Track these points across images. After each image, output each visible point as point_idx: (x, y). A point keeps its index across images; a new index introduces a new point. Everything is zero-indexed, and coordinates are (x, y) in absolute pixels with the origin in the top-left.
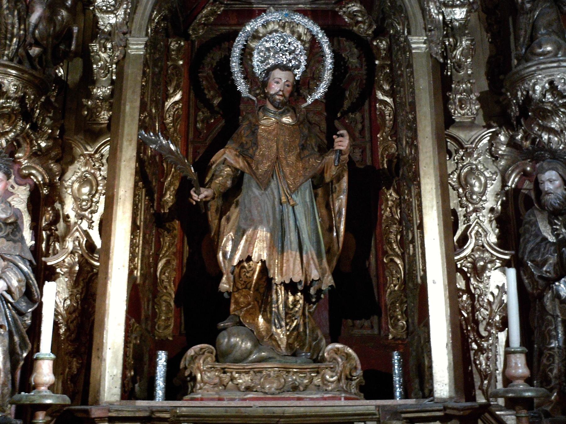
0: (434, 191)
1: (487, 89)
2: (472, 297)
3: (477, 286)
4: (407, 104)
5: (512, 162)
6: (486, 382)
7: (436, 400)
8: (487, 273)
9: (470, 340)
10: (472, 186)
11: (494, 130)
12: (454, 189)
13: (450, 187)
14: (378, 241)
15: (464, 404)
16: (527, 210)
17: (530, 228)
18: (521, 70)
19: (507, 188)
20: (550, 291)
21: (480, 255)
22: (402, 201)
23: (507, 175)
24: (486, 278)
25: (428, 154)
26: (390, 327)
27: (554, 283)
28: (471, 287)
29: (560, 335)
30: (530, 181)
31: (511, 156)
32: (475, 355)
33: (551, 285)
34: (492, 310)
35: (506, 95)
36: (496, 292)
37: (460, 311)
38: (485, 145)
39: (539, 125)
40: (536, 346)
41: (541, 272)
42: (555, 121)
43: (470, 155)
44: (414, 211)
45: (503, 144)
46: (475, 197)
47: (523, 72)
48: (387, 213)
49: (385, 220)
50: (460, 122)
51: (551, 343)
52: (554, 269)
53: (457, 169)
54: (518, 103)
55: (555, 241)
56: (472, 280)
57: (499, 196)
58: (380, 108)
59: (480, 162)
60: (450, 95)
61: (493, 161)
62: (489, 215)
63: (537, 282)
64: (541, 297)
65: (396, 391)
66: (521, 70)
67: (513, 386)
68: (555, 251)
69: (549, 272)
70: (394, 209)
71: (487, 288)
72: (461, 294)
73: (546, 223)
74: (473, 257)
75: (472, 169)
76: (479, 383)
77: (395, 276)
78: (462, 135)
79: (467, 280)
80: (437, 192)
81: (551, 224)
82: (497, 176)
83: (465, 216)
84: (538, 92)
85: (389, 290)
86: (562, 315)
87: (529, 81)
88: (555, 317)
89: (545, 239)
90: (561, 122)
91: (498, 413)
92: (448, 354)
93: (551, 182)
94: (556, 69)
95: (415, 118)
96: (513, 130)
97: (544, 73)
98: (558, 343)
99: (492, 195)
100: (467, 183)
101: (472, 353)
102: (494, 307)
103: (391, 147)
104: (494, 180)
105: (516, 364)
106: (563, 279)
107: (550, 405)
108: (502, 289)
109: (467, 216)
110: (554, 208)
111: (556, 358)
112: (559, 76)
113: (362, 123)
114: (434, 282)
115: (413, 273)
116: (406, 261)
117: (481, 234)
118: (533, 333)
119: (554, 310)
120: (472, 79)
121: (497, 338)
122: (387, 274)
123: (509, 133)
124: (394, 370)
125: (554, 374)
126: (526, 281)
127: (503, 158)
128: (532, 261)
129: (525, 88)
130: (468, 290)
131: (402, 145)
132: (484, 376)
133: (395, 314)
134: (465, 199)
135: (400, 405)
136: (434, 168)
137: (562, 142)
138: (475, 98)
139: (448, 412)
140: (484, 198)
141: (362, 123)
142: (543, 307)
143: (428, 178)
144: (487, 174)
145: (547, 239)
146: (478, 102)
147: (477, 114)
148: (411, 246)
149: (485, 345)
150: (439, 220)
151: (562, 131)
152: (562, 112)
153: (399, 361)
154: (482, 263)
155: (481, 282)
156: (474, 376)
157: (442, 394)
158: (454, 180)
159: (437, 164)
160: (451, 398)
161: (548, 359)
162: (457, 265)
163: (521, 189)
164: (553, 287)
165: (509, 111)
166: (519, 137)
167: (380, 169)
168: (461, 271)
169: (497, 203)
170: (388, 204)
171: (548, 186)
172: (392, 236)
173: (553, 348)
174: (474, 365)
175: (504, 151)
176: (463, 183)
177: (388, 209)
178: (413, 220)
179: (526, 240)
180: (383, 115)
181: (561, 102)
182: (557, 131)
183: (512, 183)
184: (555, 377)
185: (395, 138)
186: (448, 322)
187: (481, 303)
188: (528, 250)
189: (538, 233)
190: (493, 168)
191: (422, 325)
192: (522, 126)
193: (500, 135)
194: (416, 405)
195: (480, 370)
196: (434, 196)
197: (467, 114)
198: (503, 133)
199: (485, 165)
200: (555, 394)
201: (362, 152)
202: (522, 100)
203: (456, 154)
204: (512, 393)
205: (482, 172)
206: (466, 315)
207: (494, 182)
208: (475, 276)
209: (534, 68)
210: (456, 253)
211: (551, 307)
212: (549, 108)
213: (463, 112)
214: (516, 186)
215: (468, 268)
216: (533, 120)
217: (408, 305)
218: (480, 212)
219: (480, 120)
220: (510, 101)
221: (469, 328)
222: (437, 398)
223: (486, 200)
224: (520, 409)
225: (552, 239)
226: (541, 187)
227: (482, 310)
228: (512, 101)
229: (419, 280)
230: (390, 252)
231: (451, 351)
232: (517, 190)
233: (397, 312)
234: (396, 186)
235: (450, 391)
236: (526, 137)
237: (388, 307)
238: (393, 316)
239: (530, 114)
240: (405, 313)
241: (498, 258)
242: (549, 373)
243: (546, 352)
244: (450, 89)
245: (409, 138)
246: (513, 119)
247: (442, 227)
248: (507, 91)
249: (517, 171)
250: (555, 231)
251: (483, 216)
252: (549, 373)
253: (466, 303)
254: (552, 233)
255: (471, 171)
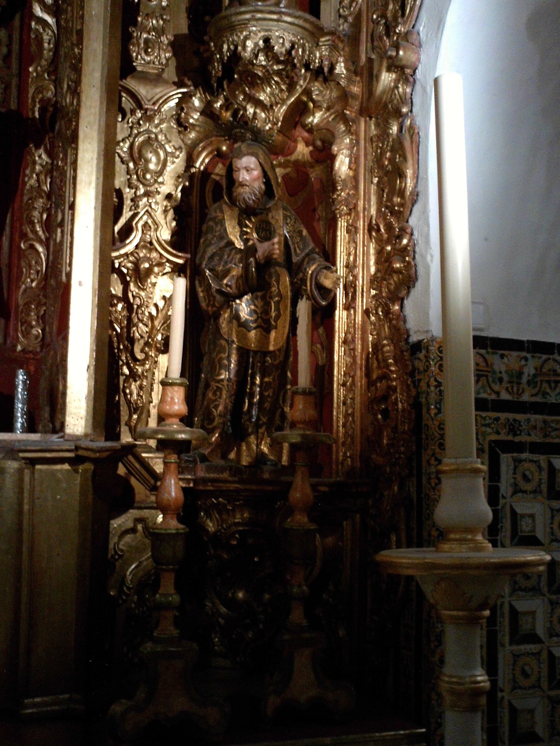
0: (95, 162)
1: (185, 31)
2: (129, 307)
3: (136, 293)
4: (74, 32)
5: (204, 137)
6: (135, 417)
7: (66, 437)
8: (153, 279)
9: (121, 363)
10: (147, 161)
11: (185, 90)
12: (123, 162)
13: (117, 158)
14: (15, 218)
15: (102, 444)
16: (215, 201)
17: (214, 226)
18: (231, 15)
19: (193, 170)
20: (229, 311)
21: (145, 255)
22: (55, 167)
23: (195, 153)
24: (150, 285)
25: (93, 110)
26: (20, 335)
27: (234, 301)
28: (130, 295)
29: (232, 365)
30: (224, 164)
31: (205, 130)
32: (125, 381)
33: (231, 303)
34: (153, 326)
35: (209, 45)
36: (161, 304)
37: (111, 323)
38: (171, 109)
39: (245, 93)
40: (203, 376)
41: (221, 285)
42: (264, 92)
43: (149, 118)
44: (68, 185)
45: (195, 110)
46: (148, 176)
47: (234, 19)
48: (33, 182)
49: (28, 190)
50: (142, 72)
51: (221, 374)
52: (236, 283)
53: (130, 136)
54: (222, 58)
55: (242, 248)
56: (132, 286)
57: (180, 180)
58: (37, 30)
59: (161, 130)
60: (134, 31)
61: (180, 132)
62: (165, 203)
63: (214, 297)
64: (217, 316)
65: (17, 421)
66: (231, 15)
67: (165, 425)
68: (241, 261)
69: (230, 287)
70: (42, 177)
71: (150, 298)
72: (115, 302)
73: (235, 222)
74: (136, 255)
75: (149, 138)
76: (126, 418)
77: (34, 268)
78: (142, 91)
79: (126, 285)
80: (98, 164)
81: (241, 225)
82: (181, 152)
83: (132, 200)
84: (249, 49)
85: (23, 286)
86: (239, 341)
87: (240, 32)
88: (230, 343)
89: (231, 244)
90: (272, 94)
91: (144, 455)
92: (89, 379)
93: (248, 170)
94: (275, 23)
95: (81, 55)
96: (212, 94)
97: (260, 25)
98: (229, 375)
99: (171, 177)
100: (141, 155)
101: (122, 378)
102: (156, 323)
103: (48, 90)
104: (177, 158)
105: (172, 398)
106: (246, 297)
107: (208, 448)
108: (168, 301)
109: (135, 200)
110: (247, 206)
111: (224, 392)
112: (277, 34)
113: (9, 46)
114: (80, 284)
115: (57, 267)
116: (51, 249)
117: (150, 227)
118: (202, 360)
119: (230, 335)
120: (167, 15)
121: (156, 362)
122: (23, 264)
123: (206, 97)
124: (17, 393)
125: (218, 412)
126: (201, 294)
127: (194, 130)
128: (210, 270)
129: (233, 40)
130: (125, 298)
131: (62, 89)
132: (134, 408)
133: (29, 319)
134: (135, 177)
135: (19, 441)
136: (99, 130)
137: (269, 120)
138: (166, 42)
139: (80, 452)
140: (161, 179)
141: (9, 46)
142: (218, 329)
143: (90, 143)
144: (169, 150)
145: (233, 244)
146: (170, 48)
147: (167, 65)
148: (59, 230)
149: (140, 370)
150: (96, 202)
151: (271, 106)
152: (275, 81)
153: (24, 382)
154: (147, 265)
155: (143, 290)
156: (122, 408)
157: (75, 430)
158: (125, 149)
159: (103, 124)
160: (86, 435)
161: (215, 394)
162: (113, 264)
163: (212, 173)
164: (232, 305)
165: (210, 68)
166: (219, 104)
167: (28, 118)
168: (119, 272)
169: (177, 188)
170: (34, 168)
171: (243, 176)
172: (36, 214)
173: (222, 380)
174: (122, 394)
175: (197, 120)
176: (136, 155)
177: (34, 176)
178: (65, 196)
179: (208, 242)
180: (39, 41)
181: (275, 67)
182: (266, 106)
183: (201, 164)
184: (220, 415)
185: (53, 77)
186: (94, 338)
187: (140, 316)
188: (208, 254)
189: (224, 235)
190: (177, 141)
191: (60, 338)
192: (223, 90)
193: (194, 98)
194: (40, 442)
195: (130, 401)
196: (95, 169)
197: (154, 63)
198: (198, 95)
199: (168, 136)
200: (217, 435)
201: (5, 89)
202: (228, 57)
203: (132, 115)
204: (162, 434)
205: (163, 145)
206: (119, 330)
207: (177, 161)
208: (136, 281)
209: (248, 16)
210: (115, 248)
211: (226, 329)
212: (260, 74)
213: (149, 59)
214: (206, 168)
215: (128, 269)
216: (239, 85)
217: (47, 308)
218: (153, 197)
219: (171, 74)
220: (213, 54)
221: (122, 347)
222: (69, 435)
223: (162, 183)
224: (170, 454)
225: (239, 244)
226: (235, 176)
227: (141, 325)
228: (216, 54)
229: (64, 278)
230: (31, 235)
231: (93, 376)
232: (206, 174)
233: (31, 316)
234: (48, 146)
235: (86, 426)
236: (227, 106)
237: (20, 309)
238: (26, 322)
239: (236, 76)
240: (42, 319)
241: (168, 261)
242: (214, 410)
243: (214, 385)
244: (135, 23)
245: (72, 82)
246: (214, 79)
247: (100, 212)
248: (211, 39)
249: (210, 149)
250: (244, 235)
251: (157, 203)
252: (214, 410)
253: (120, 314)
254: (240, 237)
255: (148, 142)
